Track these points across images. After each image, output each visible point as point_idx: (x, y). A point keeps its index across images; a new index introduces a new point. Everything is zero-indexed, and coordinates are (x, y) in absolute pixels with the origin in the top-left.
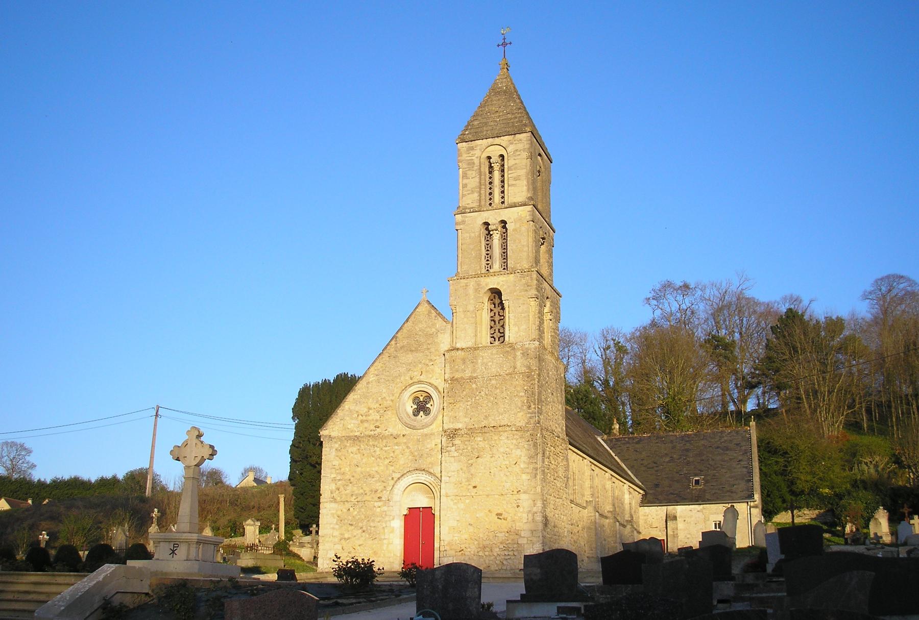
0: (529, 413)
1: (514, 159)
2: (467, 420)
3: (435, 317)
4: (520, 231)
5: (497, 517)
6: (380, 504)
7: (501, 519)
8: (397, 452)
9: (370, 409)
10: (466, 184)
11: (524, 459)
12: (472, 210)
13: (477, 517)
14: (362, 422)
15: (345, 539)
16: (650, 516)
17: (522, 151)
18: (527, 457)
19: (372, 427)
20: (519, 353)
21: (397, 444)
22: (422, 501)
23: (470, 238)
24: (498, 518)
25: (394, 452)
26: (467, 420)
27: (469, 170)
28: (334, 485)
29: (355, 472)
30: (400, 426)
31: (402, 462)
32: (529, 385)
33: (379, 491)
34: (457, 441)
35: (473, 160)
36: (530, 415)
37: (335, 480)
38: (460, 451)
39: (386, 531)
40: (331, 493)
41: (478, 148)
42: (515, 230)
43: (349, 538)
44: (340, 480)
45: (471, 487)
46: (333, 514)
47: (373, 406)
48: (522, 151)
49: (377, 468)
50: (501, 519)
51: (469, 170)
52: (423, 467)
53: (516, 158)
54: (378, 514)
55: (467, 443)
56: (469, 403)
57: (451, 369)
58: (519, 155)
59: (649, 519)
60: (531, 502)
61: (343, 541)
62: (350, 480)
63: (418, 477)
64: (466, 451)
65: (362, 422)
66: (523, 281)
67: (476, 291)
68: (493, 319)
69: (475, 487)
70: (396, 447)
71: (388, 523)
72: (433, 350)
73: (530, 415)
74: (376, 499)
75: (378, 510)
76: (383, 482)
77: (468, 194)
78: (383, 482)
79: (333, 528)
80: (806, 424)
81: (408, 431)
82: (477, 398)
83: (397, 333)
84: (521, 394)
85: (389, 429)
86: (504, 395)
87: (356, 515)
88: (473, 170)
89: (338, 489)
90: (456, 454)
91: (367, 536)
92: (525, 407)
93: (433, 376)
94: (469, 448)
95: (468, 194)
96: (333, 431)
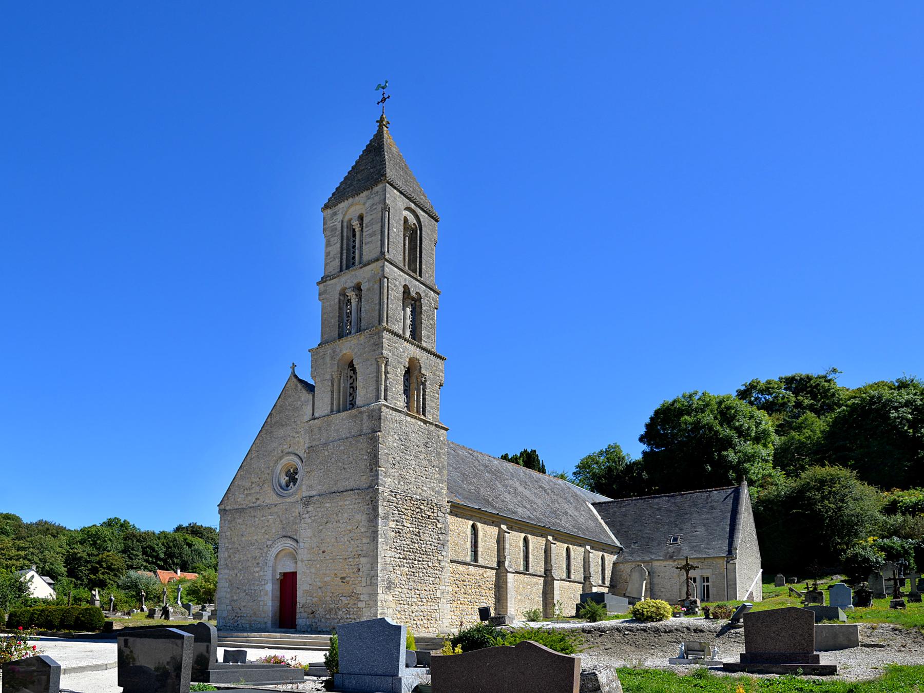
0: (371, 476)
1: (371, 215)
2: (320, 487)
3: (301, 390)
4: (373, 289)
5: (341, 581)
6: (258, 569)
7: (344, 582)
8: (271, 521)
9: (252, 483)
10: (329, 252)
11: (364, 523)
12: (332, 277)
13: (325, 582)
14: (247, 495)
15: (234, 601)
16: (624, 572)
17: (378, 204)
18: (366, 521)
19: (254, 500)
20: (365, 416)
21: (271, 514)
22: (289, 569)
23: (330, 307)
24: (342, 582)
25: (268, 521)
26: (320, 487)
27: (331, 237)
28: (227, 553)
29: (241, 541)
30: (275, 496)
31: (274, 531)
32: (371, 447)
33: (258, 558)
34: (310, 509)
35: (335, 225)
36: (372, 478)
37: (228, 549)
38: (313, 518)
39: (262, 593)
40: (225, 561)
41: (340, 212)
42: (369, 290)
43: (237, 600)
44: (231, 549)
45: (321, 552)
46: (226, 579)
47: (254, 480)
48: (378, 204)
49: (255, 538)
50: (344, 582)
51: (331, 237)
52: (289, 534)
53: (372, 213)
54: (257, 578)
55: (318, 509)
56: (322, 471)
57: (310, 439)
58: (376, 208)
59: (624, 575)
60: (369, 565)
61: (232, 603)
62: (237, 548)
63: (286, 545)
64: (317, 517)
65: (247, 495)
66: (372, 341)
67: (332, 359)
68: (352, 385)
69: (324, 552)
70: (270, 517)
71: (263, 586)
72: (298, 422)
73: (372, 478)
74: (255, 564)
75: (257, 575)
76: (260, 549)
77: (331, 262)
78: (260, 549)
79: (226, 592)
80: (804, 645)
81: (279, 500)
82: (329, 465)
83: (272, 410)
84: (364, 458)
85: (266, 501)
86: (351, 459)
87: (241, 579)
88: (335, 236)
89: (230, 557)
90: (309, 521)
91: (249, 598)
92: (368, 471)
93: (299, 447)
94: (320, 515)
95: (331, 262)
96: (227, 506)
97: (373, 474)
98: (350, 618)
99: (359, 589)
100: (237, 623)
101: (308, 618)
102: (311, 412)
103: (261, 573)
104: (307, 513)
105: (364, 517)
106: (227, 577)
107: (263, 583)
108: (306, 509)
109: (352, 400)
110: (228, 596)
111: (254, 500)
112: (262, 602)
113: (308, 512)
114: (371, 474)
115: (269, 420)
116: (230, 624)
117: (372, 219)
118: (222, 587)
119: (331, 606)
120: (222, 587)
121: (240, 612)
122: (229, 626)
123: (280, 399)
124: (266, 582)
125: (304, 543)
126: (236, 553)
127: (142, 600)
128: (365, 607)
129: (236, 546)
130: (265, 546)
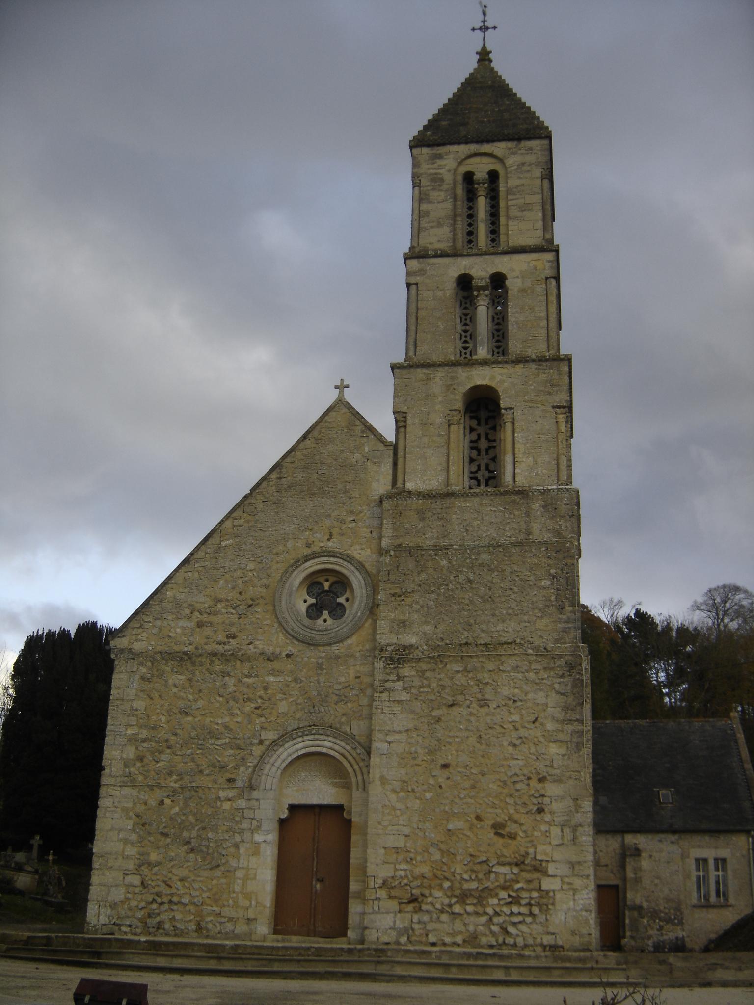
6: (230, 794)
13: (449, 830)
15: (149, 864)
19: (221, 637)
38: (413, 691)
39: (242, 850)
42: (523, 291)
43: (158, 864)
46: (126, 810)
65: (200, 625)
68: (475, 445)
69: (445, 766)
75: (227, 806)
79: (126, 841)
89: (141, 759)
90: (404, 696)
95: (432, 227)
97: (564, 617)
98: (520, 914)
99: (542, 851)
100: (158, 919)
101: (400, 912)
102: (390, 477)
103: (242, 803)
104: (398, 680)
105: (553, 699)
106: (130, 805)
107: (245, 825)
108: (395, 671)
109: (476, 472)
110: (131, 851)
111: (221, 637)
112: (244, 871)
113: (399, 678)
114: (560, 616)
115: (274, 476)
116: (135, 922)
117: (523, 185)
118: (112, 829)
119: (466, 886)
120: (112, 829)
121: (167, 891)
122: (130, 926)
123: (307, 442)
124: (255, 823)
125: (389, 743)
126: (160, 752)
127: (66, 883)
128: (562, 889)
129: (162, 734)
130: (256, 741)
